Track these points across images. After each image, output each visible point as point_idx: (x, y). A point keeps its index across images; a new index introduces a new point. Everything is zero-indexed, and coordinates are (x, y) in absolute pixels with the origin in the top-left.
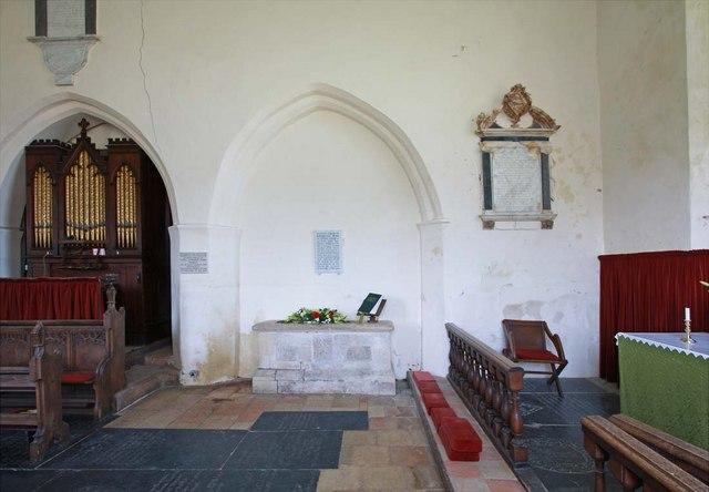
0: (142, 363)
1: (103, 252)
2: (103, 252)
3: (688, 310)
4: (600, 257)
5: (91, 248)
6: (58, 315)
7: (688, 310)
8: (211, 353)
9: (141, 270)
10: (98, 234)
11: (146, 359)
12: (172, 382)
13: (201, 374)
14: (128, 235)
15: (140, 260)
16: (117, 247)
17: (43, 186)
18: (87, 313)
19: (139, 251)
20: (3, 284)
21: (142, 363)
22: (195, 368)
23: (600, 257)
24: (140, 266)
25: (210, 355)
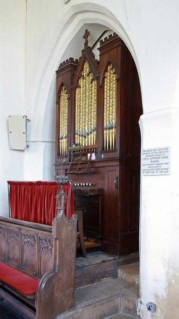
0: (115, 275)
1: (94, 157)
2: (94, 157)
3: (97, 58)
4: (9, 183)
5: (85, 155)
6: (19, 216)
7: (97, 58)
8: (170, 284)
9: (117, 174)
10: (91, 140)
11: (119, 271)
12: (130, 310)
13: (159, 310)
14: (111, 136)
15: (118, 163)
16: (103, 150)
17: (64, 96)
18: (32, 217)
19: (117, 154)
20: (23, 188)
21: (115, 275)
22: (153, 301)
23: (9, 183)
24: (118, 168)
25: (168, 287)
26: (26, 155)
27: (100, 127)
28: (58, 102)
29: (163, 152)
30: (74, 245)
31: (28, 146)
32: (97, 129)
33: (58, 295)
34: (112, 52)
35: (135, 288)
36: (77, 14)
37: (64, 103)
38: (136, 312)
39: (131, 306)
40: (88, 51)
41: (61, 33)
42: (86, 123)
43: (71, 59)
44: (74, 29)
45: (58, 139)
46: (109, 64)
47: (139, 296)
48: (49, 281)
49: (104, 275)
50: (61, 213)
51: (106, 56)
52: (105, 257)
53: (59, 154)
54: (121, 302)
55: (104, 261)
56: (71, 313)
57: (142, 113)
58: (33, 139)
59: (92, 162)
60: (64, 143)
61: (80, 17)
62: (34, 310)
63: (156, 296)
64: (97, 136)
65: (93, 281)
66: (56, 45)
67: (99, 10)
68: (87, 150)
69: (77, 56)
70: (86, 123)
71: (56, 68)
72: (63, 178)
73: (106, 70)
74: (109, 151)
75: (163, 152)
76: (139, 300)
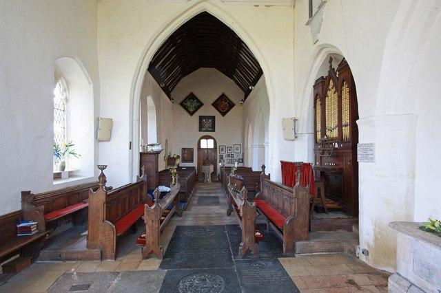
1: (336, 146)
2: (336, 146)
10: (335, 134)
12: (352, 252)
17: (319, 102)
26: (296, 143)
27: (340, 125)
28: (315, 107)
29: (370, 146)
30: (308, 203)
31: (296, 137)
32: (338, 126)
33: (297, 230)
34: (345, 73)
35: (357, 238)
36: (322, 49)
37: (319, 107)
38: (355, 253)
39: (352, 250)
40: (332, 70)
41: (314, 61)
42: (332, 122)
43: (322, 77)
44: (322, 57)
45: (316, 132)
46: (344, 81)
47: (358, 244)
48: (291, 221)
49: (340, 227)
50: (298, 184)
51: (342, 75)
52: (341, 215)
53: (316, 142)
54: (346, 246)
55: (339, 218)
56: (306, 243)
57: (358, 118)
58: (300, 132)
59: (336, 149)
60: (319, 136)
61: (324, 51)
62: (282, 233)
63: (369, 246)
64: (339, 131)
65: (330, 230)
66: (312, 68)
67: (333, 47)
68: (333, 140)
69: (325, 74)
70: (332, 122)
71: (313, 84)
72: (27, 207)
73: (342, 85)
74: (346, 142)
75: (370, 146)
76: (358, 246)
